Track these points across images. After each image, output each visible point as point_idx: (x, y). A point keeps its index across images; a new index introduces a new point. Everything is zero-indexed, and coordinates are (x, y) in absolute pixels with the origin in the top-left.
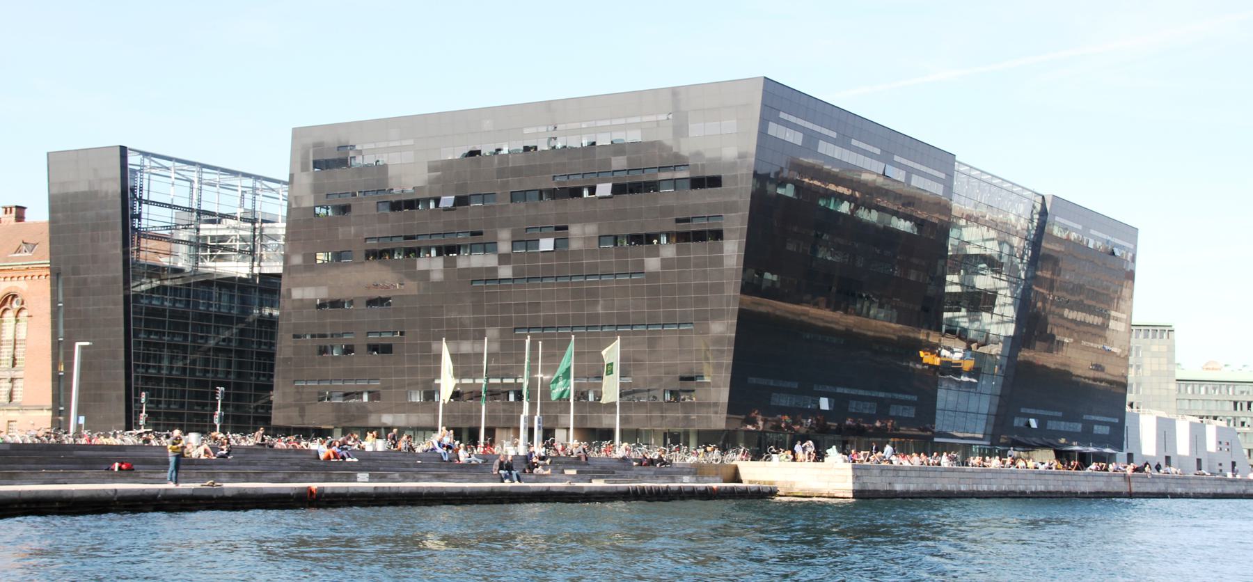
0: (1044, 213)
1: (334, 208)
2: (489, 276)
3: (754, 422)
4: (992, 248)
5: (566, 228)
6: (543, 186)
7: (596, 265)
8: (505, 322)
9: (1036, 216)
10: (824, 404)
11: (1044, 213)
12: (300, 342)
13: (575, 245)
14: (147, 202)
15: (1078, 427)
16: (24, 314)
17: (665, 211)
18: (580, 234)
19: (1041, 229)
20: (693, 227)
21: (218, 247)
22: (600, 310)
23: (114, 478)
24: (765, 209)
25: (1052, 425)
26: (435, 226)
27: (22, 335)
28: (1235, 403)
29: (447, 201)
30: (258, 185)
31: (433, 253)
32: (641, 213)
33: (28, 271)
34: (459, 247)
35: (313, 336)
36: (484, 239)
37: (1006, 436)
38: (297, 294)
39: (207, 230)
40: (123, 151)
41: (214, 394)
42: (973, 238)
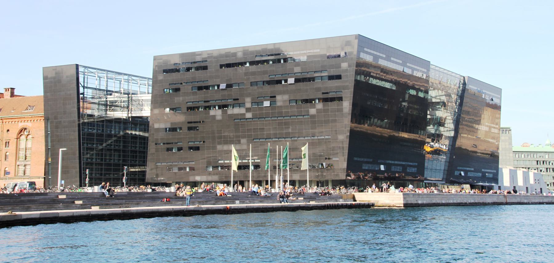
0: (464, 84)
1: (172, 89)
2: (242, 117)
3: (350, 176)
4: (444, 98)
5: (275, 97)
6: (265, 80)
7: (288, 112)
8: (249, 136)
9: (461, 85)
10: (382, 168)
11: (464, 84)
12: (158, 146)
13: (279, 104)
14: (87, 88)
15: (480, 175)
16: (30, 137)
17: (318, 89)
18: (281, 99)
19: (464, 90)
20: (330, 95)
21: (112, 105)
22: (290, 130)
23: (165, 204)
24: (363, 90)
25: (470, 174)
26: (218, 96)
27: (29, 145)
28: (537, 161)
29: (223, 86)
30: (86, 71)
31: (217, 108)
32: (307, 90)
33: (32, 118)
34: (228, 105)
35: (164, 144)
36: (240, 102)
37: (451, 179)
38: (156, 126)
39: (110, 98)
41: (123, 169)
42: (434, 95)
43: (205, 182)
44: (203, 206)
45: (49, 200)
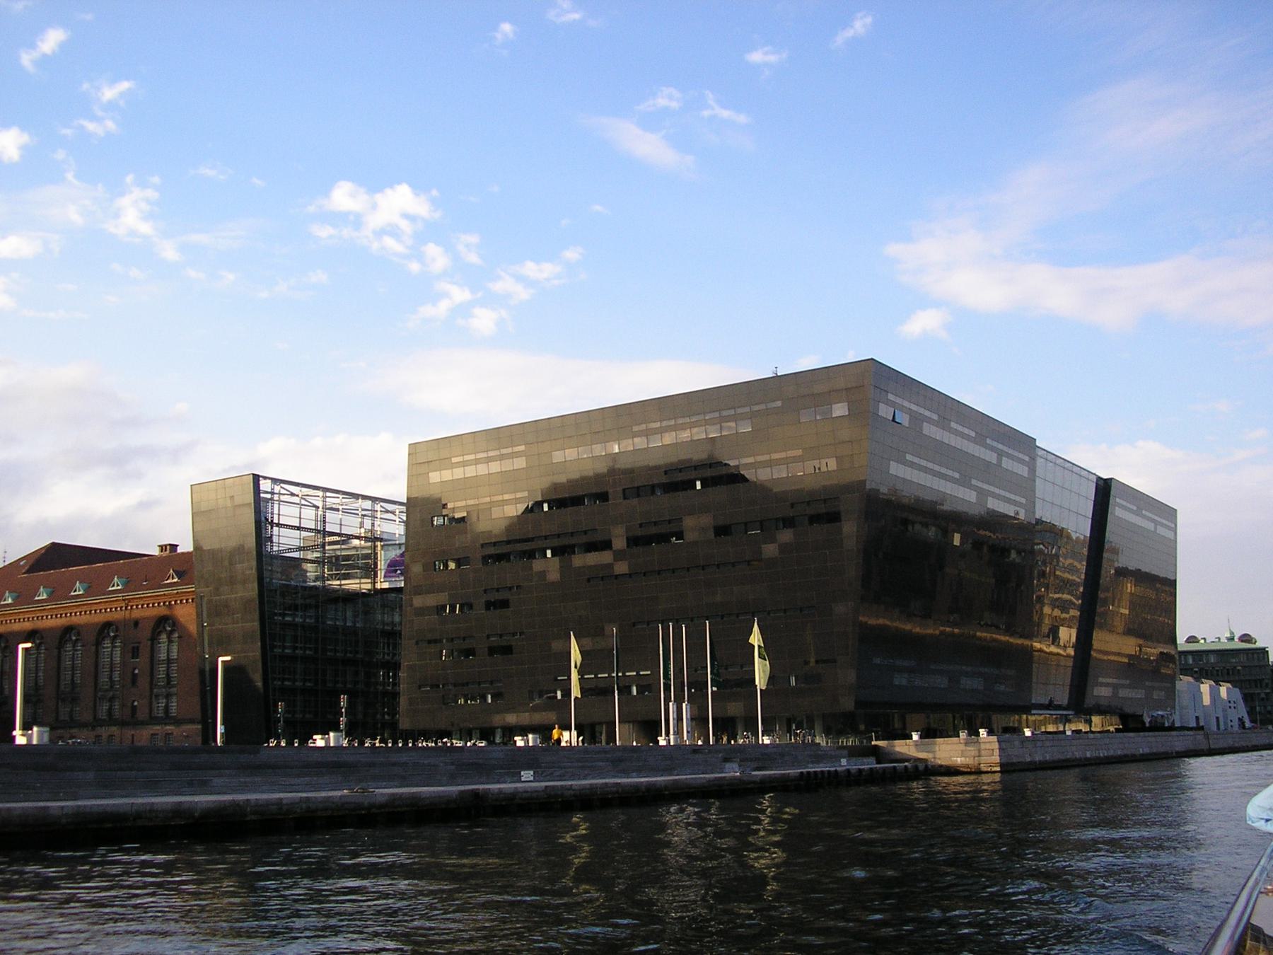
2: (603, 575)
14: (278, 525)
27: (174, 655)
40: (256, 478)
43: (781, 787)
44: (197, 799)
45: (751, 786)
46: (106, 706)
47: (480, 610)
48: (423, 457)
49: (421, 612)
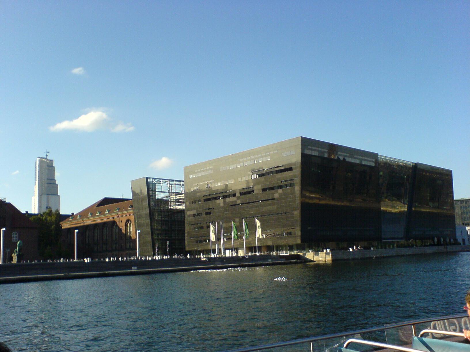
40: (147, 179)
46: (128, 245)
47: (204, 215)
48: (188, 171)
49: (189, 216)
